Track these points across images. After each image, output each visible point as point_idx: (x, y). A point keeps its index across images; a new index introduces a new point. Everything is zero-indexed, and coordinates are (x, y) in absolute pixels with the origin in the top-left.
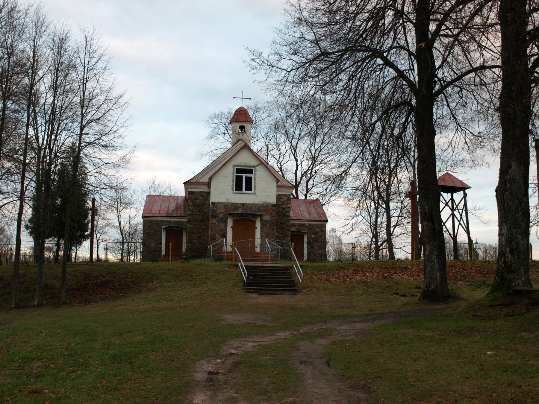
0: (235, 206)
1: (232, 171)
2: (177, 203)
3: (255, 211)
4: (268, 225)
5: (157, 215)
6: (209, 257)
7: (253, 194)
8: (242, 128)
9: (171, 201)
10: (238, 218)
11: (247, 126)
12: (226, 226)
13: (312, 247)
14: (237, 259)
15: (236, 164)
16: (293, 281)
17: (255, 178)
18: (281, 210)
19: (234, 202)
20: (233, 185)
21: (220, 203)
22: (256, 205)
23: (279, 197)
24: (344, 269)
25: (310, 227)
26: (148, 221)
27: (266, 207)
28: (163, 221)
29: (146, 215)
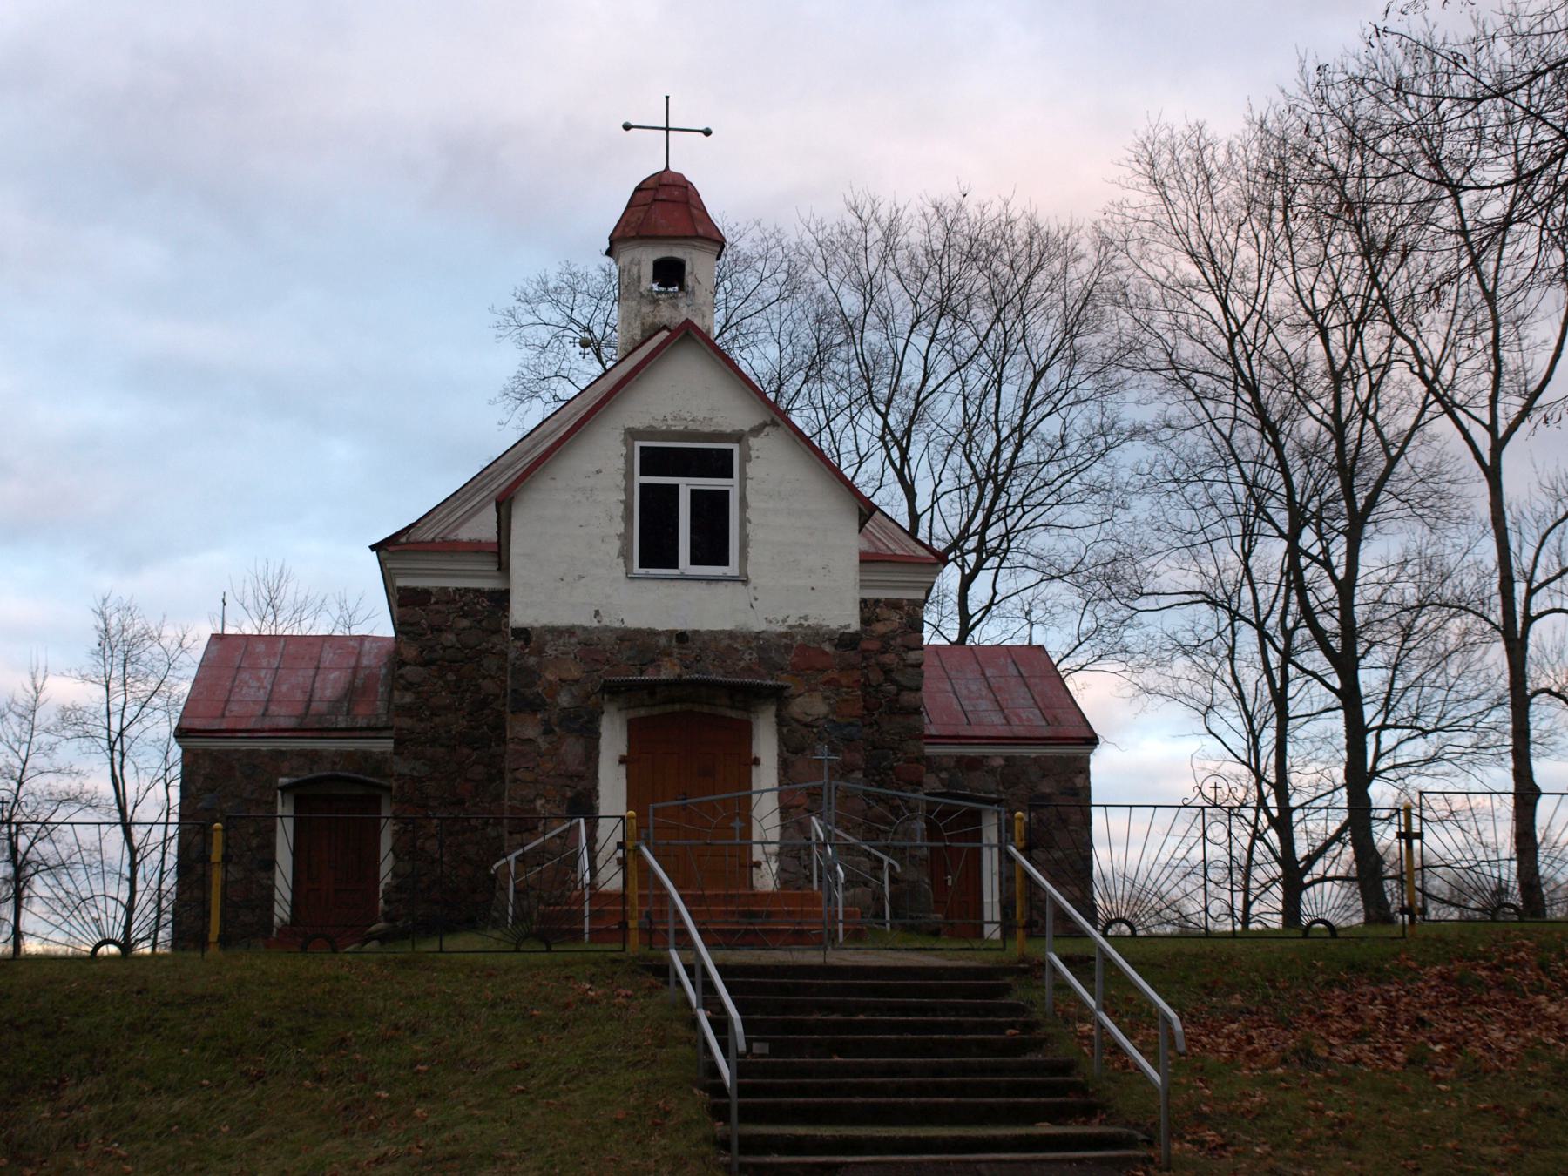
0: (641, 644)
1: (621, 463)
2: (356, 669)
3: (749, 670)
5: (251, 724)
6: (497, 924)
7: (732, 579)
8: (670, 273)
9: (328, 657)
10: (656, 711)
11: (698, 264)
14: (660, 927)
15: (638, 424)
16: (1066, 1068)
18: (876, 677)
19: (632, 622)
20: (626, 537)
23: (868, 608)
24: (1379, 977)
26: (207, 753)
27: (803, 648)
28: (279, 754)
29: (198, 724)
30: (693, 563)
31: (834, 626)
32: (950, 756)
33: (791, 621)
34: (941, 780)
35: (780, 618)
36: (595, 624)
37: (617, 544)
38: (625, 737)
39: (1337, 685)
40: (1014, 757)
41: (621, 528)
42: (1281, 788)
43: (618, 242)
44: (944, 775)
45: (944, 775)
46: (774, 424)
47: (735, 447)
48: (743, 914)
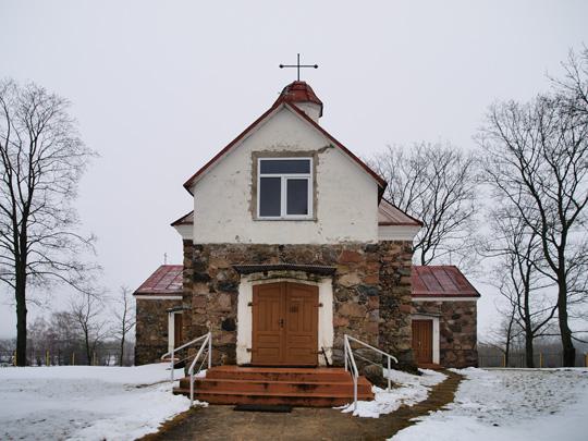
4: (356, 299)
12: (234, 302)
13: (450, 340)
15: (260, 148)
17: (315, 183)
18: (390, 271)
19: (255, 242)
20: (253, 202)
21: (216, 246)
22: (318, 248)
26: (144, 300)
27: (347, 252)
30: (288, 213)
31: (364, 241)
36: (236, 242)
37: (248, 205)
39: (556, 278)
42: (526, 309)
46: (331, 146)
47: (311, 159)
48: (300, 386)
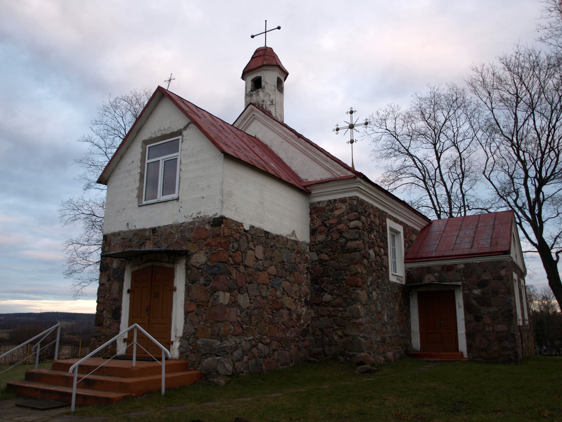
3: (177, 242)
4: (202, 281)
10: (141, 267)
13: (478, 319)
20: (140, 189)
25: (468, 270)
27: (198, 228)
31: (211, 215)
32: (438, 266)
33: (194, 216)
34: (435, 277)
35: (190, 215)
37: (136, 192)
38: (130, 283)
40: (469, 264)
41: (138, 185)
43: (243, 77)
44: (436, 274)
45: (436, 274)
